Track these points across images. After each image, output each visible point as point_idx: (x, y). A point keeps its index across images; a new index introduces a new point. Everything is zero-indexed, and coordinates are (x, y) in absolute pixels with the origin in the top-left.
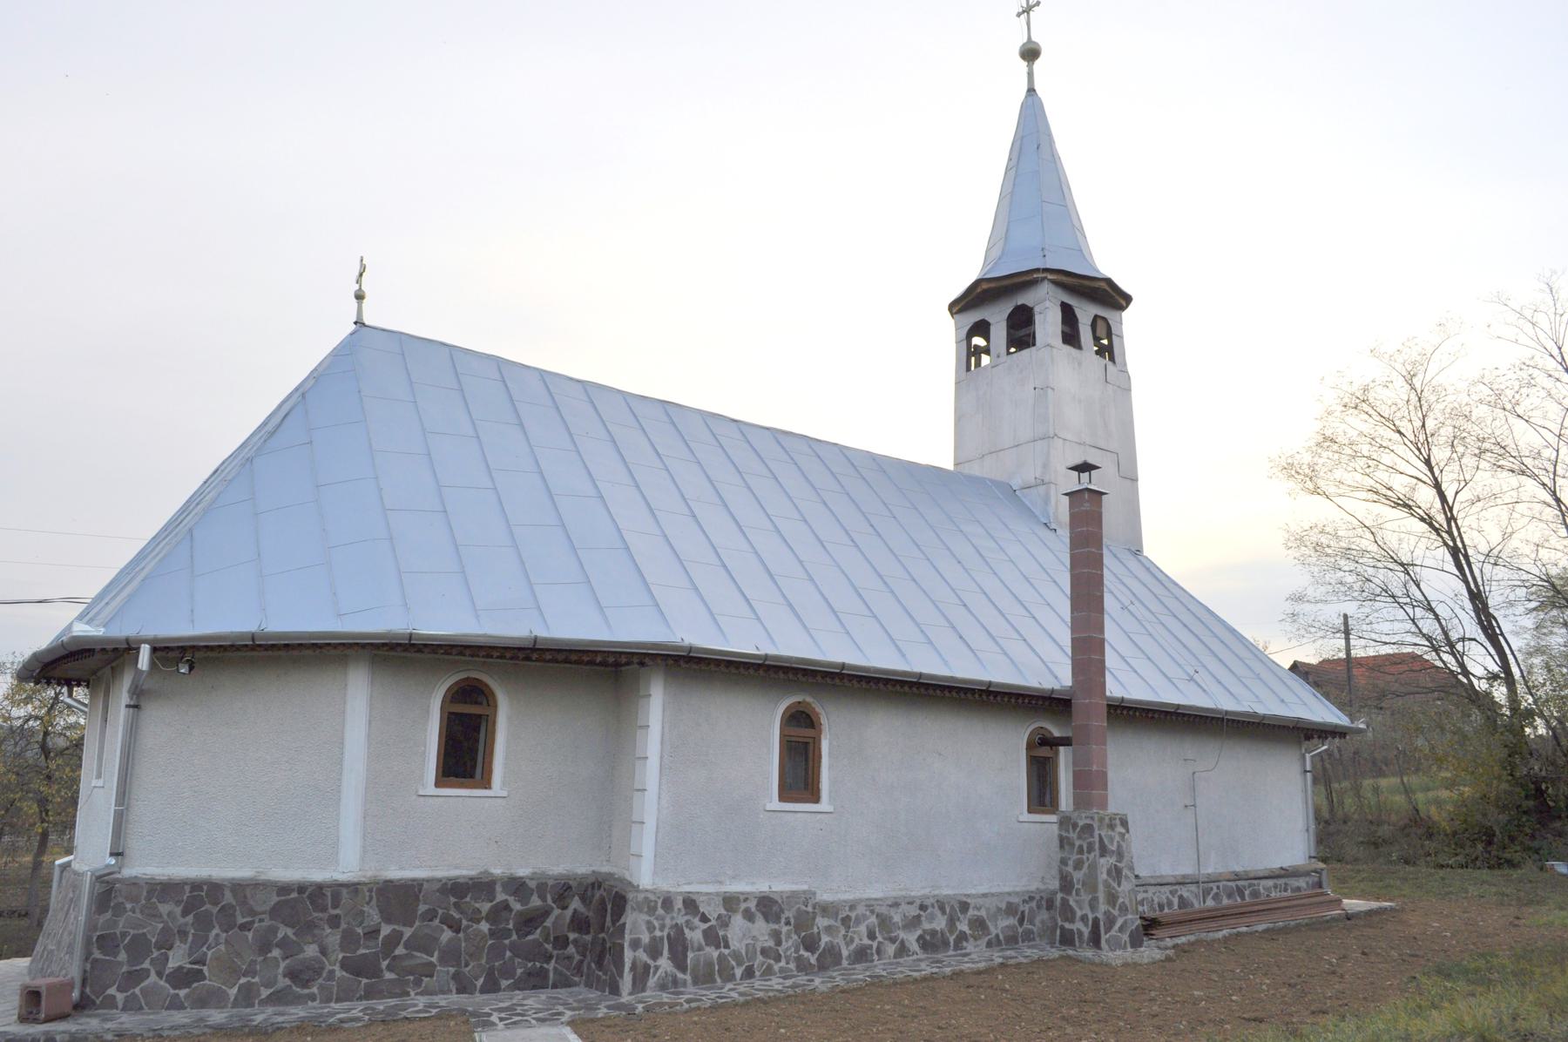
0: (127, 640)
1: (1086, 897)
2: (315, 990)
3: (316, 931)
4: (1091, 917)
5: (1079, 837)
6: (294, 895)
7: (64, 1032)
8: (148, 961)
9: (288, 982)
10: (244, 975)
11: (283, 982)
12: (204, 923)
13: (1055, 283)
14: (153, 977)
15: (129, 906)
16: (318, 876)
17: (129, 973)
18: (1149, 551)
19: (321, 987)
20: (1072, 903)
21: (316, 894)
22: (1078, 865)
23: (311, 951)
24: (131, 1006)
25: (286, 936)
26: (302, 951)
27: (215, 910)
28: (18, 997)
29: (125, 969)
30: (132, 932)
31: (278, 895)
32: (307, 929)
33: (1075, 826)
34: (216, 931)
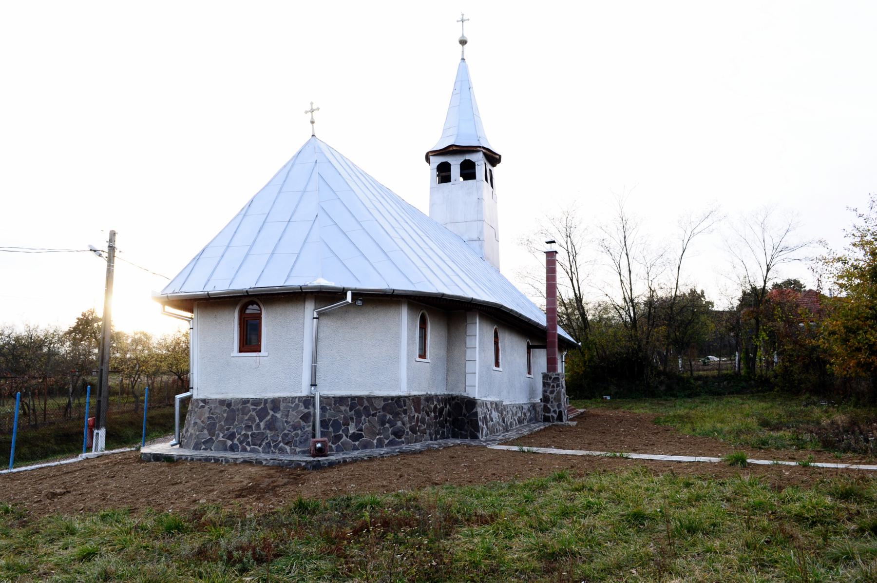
0: (344, 288)
1: (555, 404)
2: (403, 439)
3: (400, 416)
4: (558, 410)
5: (553, 382)
6: (390, 401)
7: (350, 458)
8: (341, 431)
9: (393, 437)
10: (378, 435)
11: (392, 437)
12: (359, 414)
13: (484, 153)
14: (344, 438)
15: (328, 408)
16: (394, 393)
17: (335, 436)
18: (501, 272)
19: (405, 438)
20: (549, 406)
21: (398, 400)
22: (552, 392)
23: (399, 424)
24: (339, 450)
25: (390, 419)
26: (396, 424)
27: (362, 408)
29: (333, 435)
30: (333, 419)
31: (384, 401)
32: (396, 415)
33: (550, 378)
34: (363, 417)
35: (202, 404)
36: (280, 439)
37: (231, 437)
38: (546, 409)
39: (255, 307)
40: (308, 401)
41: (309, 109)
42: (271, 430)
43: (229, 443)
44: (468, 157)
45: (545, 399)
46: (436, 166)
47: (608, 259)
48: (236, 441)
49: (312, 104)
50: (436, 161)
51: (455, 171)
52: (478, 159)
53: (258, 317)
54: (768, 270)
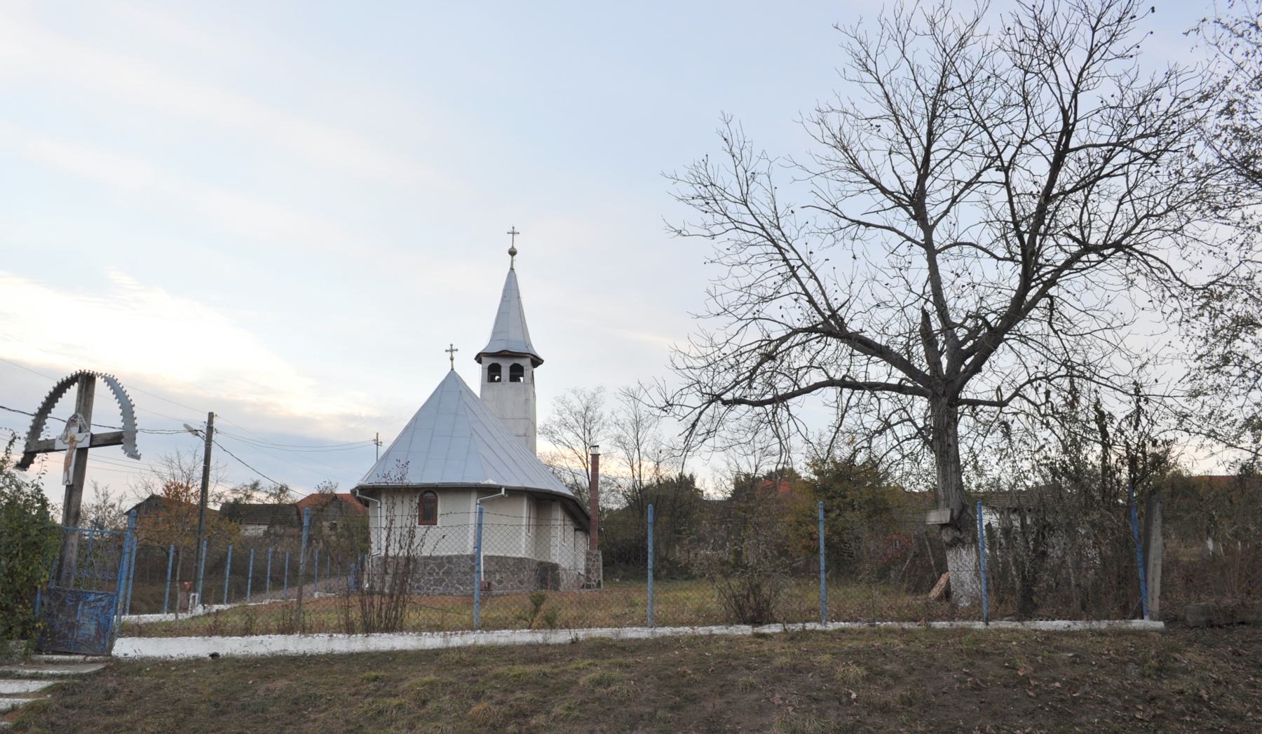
1: (596, 575)
11: (518, 584)
16: (520, 555)
28: (295, 651)
38: (588, 579)
39: (432, 495)
40: (474, 558)
41: (449, 348)
44: (517, 361)
45: (588, 571)
46: (487, 365)
47: (622, 453)
49: (451, 345)
50: (488, 362)
51: (505, 372)
52: (525, 363)
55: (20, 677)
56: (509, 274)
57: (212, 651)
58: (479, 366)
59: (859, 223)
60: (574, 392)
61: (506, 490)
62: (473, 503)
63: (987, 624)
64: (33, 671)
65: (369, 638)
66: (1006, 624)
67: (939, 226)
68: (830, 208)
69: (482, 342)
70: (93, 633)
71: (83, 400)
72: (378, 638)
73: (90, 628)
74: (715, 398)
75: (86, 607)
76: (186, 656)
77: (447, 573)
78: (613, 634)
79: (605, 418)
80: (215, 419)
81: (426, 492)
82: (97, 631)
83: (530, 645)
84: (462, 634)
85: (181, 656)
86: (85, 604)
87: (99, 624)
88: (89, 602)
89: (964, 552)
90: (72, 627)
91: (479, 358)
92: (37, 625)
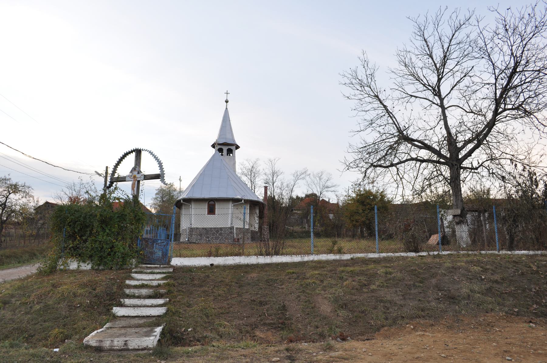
35: (196, 229)
36: (224, 238)
37: (208, 238)
40: (232, 228)
42: (221, 236)
43: (207, 239)
44: (230, 147)
48: (210, 239)
51: (225, 152)
52: (233, 148)
53: (214, 205)
54: (320, 194)
55: (146, 273)
56: (225, 110)
57: (211, 263)
58: (214, 150)
59: (412, 96)
60: (247, 160)
61: (244, 201)
62: (230, 205)
63: (499, 252)
64: (150, 271)
65: (273, 258)
66: (504, 252)
67: (446, 98)
68: (397, 87)
69: (214, 138)
70: (161, 255)
71: (138, 161)
72: (276, 258)
73: (159, 254)
74: (372, 165)
75: (157, 245)
76: (201, 265)
77: (221, 234)
78: (365, 256)
79: (260, 171)
80: (108, 169)
81: (210, 201)
82: (163, 255)
83: (335, 261)
84: (308, 256)
85: (199, 265)
86: (156, 244)
87: (163, 252)
88: (159, 243)
89: (463, 226)
90: (152, 253)
91: (213, 146)
92: (141, 253)
